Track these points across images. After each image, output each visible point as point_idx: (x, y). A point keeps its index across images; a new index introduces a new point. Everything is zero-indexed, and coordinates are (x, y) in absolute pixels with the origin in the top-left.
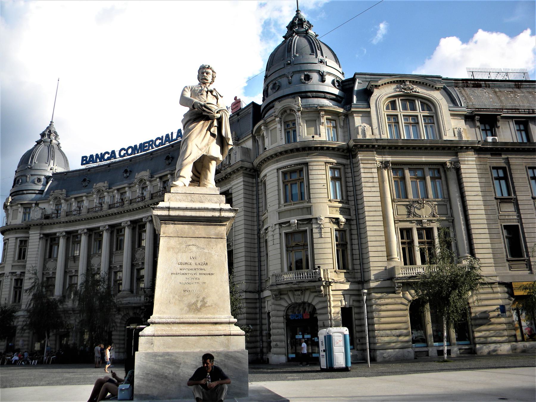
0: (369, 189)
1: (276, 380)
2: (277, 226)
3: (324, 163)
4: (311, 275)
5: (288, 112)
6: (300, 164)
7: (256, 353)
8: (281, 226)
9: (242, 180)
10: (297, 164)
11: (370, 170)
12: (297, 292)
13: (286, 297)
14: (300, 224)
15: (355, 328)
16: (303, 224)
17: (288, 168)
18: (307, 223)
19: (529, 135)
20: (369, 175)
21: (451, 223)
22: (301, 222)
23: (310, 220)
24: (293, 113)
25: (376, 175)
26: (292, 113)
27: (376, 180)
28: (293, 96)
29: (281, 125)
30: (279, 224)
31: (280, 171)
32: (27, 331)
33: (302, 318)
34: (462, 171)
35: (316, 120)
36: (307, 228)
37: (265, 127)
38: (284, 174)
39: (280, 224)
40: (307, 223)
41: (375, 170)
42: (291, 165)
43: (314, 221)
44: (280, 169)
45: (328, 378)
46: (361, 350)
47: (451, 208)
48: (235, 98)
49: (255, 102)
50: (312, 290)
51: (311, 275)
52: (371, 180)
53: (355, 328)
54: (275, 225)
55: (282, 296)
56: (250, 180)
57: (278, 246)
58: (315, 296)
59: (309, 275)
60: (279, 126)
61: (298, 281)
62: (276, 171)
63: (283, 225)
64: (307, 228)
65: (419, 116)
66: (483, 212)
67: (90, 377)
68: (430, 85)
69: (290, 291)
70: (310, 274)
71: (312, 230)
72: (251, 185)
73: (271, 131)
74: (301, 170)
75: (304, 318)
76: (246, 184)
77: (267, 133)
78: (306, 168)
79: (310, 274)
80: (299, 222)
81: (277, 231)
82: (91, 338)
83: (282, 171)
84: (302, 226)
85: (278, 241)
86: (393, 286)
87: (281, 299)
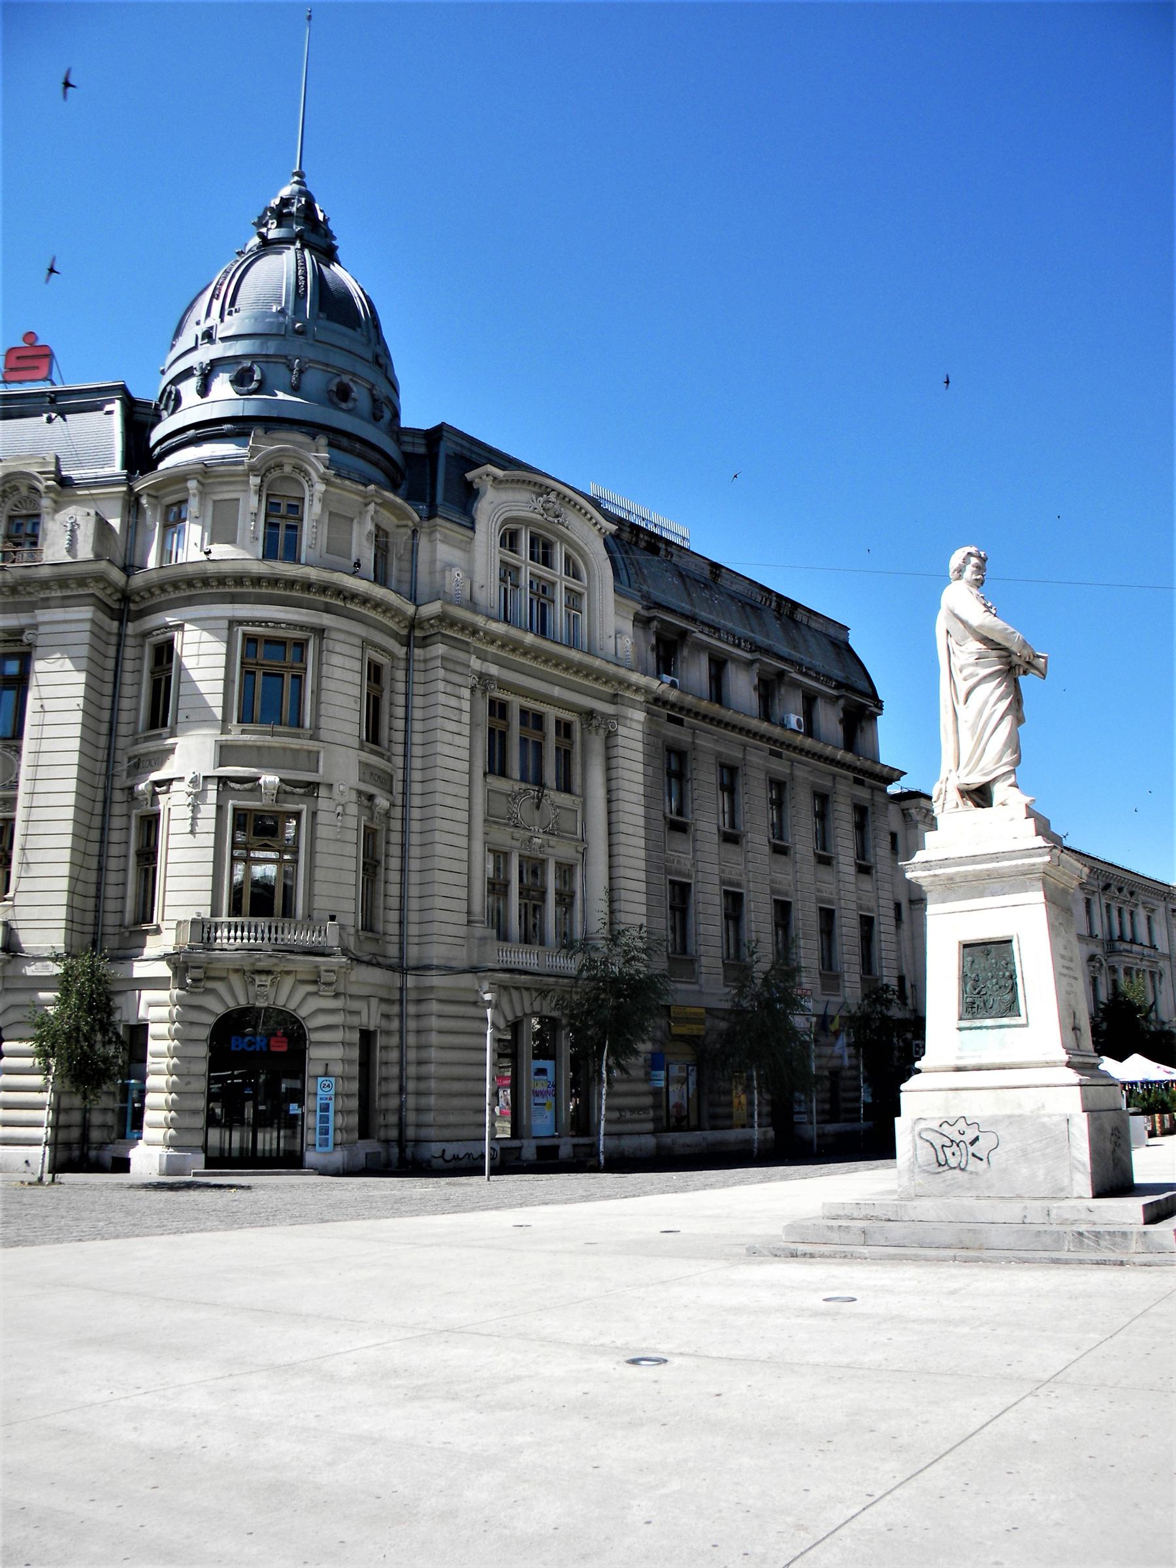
0: (448, 737)
2: (212, 786)
3: (358, 642)
4: (266, 935)
6: (302, 627)
8: (225, 784)
9: (89, 615)
10: (296, 625)
11: (457, 691)
12: (264, 977)
13: (219, 986)
14: (286, 792)
17: (267, 626)
18: (304, 795)
19: (723, 689)
20: (453, 702)
21: (581, 856)
22: (288, 788)
23: (311, 788)
25: (466, 706)
27: (466, 718)
28: (313, 430)
29: (260, 501)
30: (220, 778)
31: (240, 630)
33: (265, 1049)
35: (352, 520)
36: (303, 807)
37: (200, 487)
39: (222, 780)
40: (304, 795)
41: (466, 693)
42: (277, 623)
43: (323, 792)
44: (241, 622)
47: (584, 821)
49: (128, 386)
50: (300, 977)
51: (266, 935)
52: (453, 715)
53: (380, 1084)
54: (205, 778)
55: (210, 985)
56: (105, 620)
57: (210, 840)
58: (309, 994)
59: (260, 935)
60: (254, 500)
61: (277, 947)
62: (225, 624)
63: (233, 785)
64: (303, 807)
66: (642, 843)
67: (811, 1101)
69: (236, 971)
70: (263, 932)
71: (314, 814)
75: (273, 1049)
76: (97, 630)
77: (202, 504)
78: (317, 641)
79: (263, 932)
80: (284, 786)
82: (588, 1030)
83: (244, 635)
84: (290, 798)
85: (210, 826)
86: (477, 987)
87: (208, 991)
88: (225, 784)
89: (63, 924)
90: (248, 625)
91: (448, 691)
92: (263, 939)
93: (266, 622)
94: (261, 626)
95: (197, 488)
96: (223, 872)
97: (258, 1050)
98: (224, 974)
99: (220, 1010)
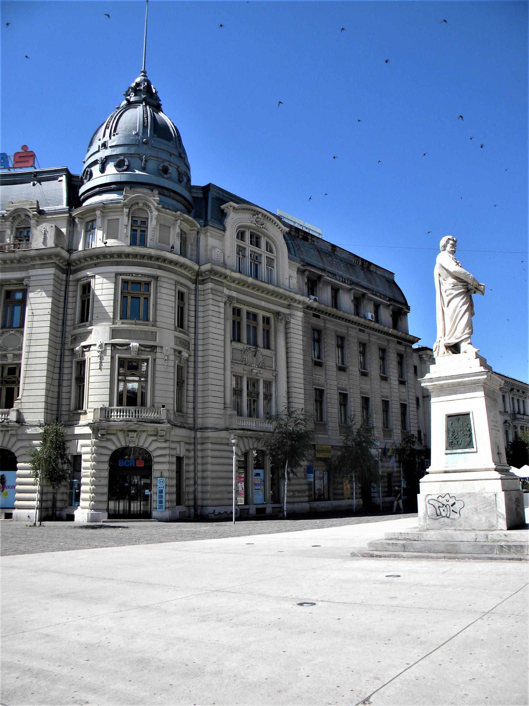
1: (357, 523)
2: (109, 348)
3: (173, 282)
4: (134, 414)
5: (141, 205)
6: (148, 276)
7: (47, 509)
8: (114, 347)
11: (218, 304)
12: (133, 433)
13: (113, 438)
14: (142, 350)
15: (185, 481)
16: (145, 351)
20: (216, 309)
21: (274, 378)
22: (143, 348)
24: (146, 209)
25: (222, 310)
26: (146, 209)
27: (222, 316)
31: (121, 277)
32: (371, 462)
34: (292, 325)
35: (170, 227)
36: (150, 357)
38: (125, 282)
39: (114, 345)
40: (150, 351)
41: (222, 305)
42: (137, 274)
43: (158, 350)
44: (121, 274)
45: (319, 527)
46: (187, 506)
47: (276, 362)
48: (24, 147)
50: (149, 433)
53: (185, 481)
55: (109, 437)
57: (108, 372)
59: (131, 415)
62: (114, 275)
63: (118, 347)
64: (150, 357)
65: (263, 256)
68: (277, 226)
69: (121, 431)
70: (132, 413)
71: (155, 360)
72: (59, 281)
73: (108, 220)
74: (148, 284)
75: (137, 465)
76: (56, 278)
77: (102, 222)
79: (132, 413)
81: (109, 352)
83: (122, 278)
85: (108, 365)
86: (228, 437)
87: (108, 440)
88: (114, 347)
89: (43, 410)
90: (124, 275)
91: (214, 304)
92: (132, 416)
93: (132, 274)
94: (129, 276)
95: (100, 214)
96: (114, 388)
97: (131, 466)
98: (115, 432)
99: (114, 448)
